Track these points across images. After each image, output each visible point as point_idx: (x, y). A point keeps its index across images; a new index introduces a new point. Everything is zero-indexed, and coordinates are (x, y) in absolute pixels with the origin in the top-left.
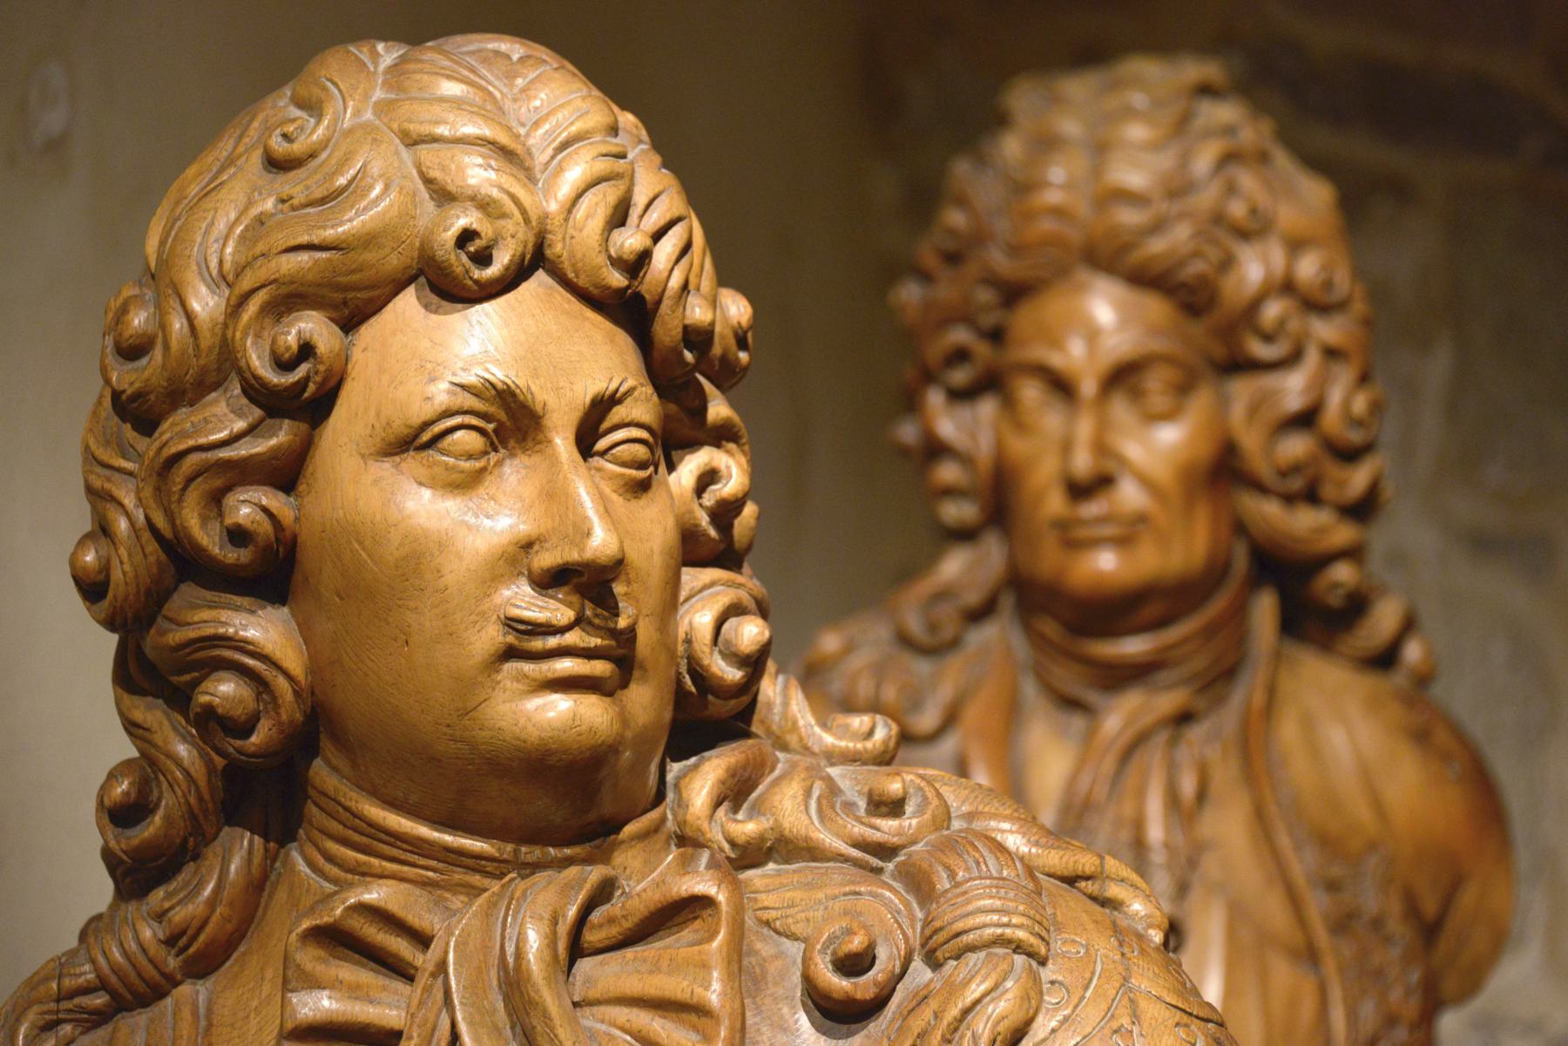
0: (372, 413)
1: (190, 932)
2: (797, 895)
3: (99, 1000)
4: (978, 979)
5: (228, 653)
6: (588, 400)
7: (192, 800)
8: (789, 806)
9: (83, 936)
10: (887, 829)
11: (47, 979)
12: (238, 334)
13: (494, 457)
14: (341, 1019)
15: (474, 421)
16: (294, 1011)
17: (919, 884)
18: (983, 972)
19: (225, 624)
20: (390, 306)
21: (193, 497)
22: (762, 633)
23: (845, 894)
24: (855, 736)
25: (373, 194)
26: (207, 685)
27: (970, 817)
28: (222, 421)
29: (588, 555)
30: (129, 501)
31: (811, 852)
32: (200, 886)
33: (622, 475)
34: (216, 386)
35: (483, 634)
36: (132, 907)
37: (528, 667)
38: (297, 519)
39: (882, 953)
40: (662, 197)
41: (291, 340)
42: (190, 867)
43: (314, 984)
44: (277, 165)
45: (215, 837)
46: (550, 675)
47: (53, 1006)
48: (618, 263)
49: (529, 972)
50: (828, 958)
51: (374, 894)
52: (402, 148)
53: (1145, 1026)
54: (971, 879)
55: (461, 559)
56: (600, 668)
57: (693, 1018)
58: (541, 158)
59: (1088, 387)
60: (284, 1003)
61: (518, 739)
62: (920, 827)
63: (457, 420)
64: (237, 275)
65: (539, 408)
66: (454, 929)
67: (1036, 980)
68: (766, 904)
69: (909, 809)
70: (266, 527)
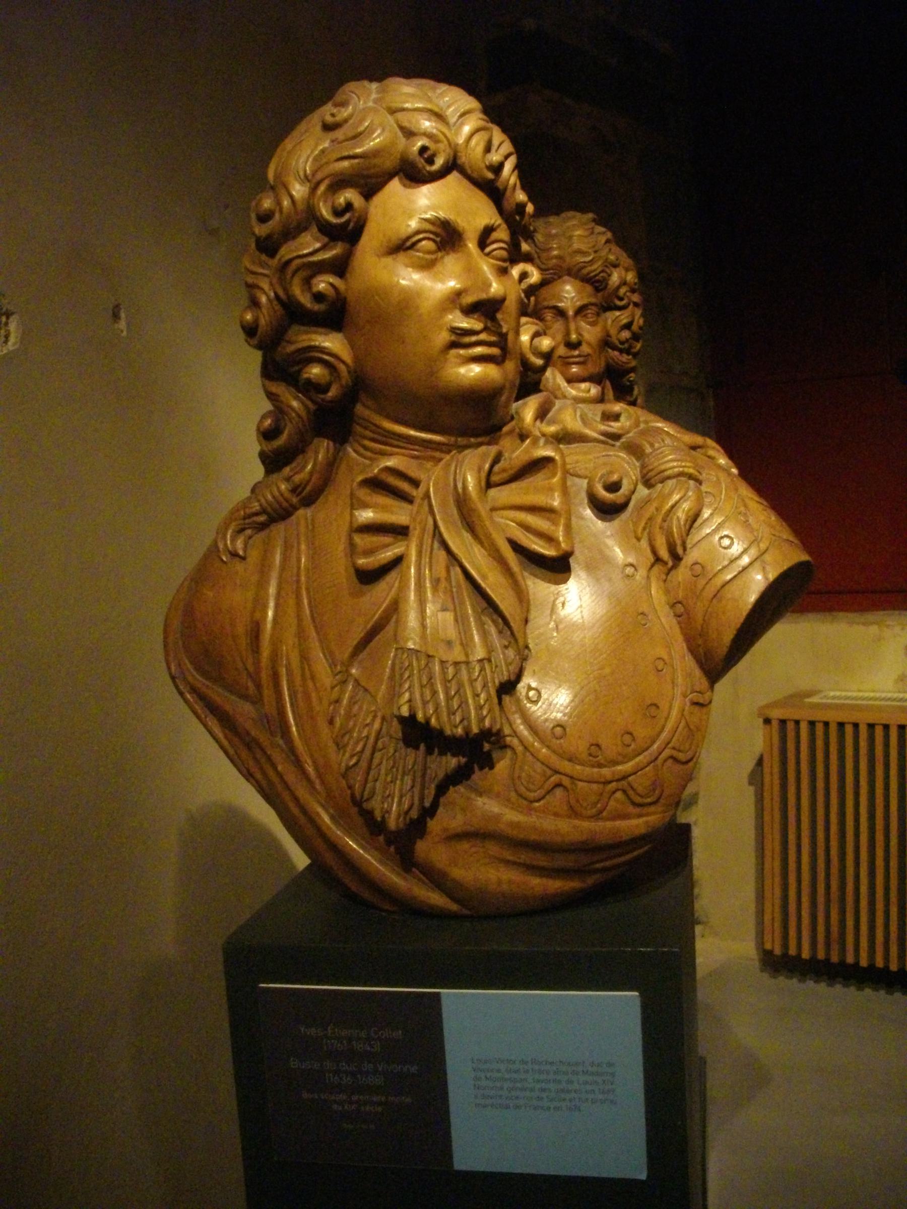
0: (381, 235)
2: (580, 457)
3: (262, 518)
4: (676, 492)
6: (482, 227)
7: (300, 425)
8: (569, 418)
9: (253, 490)
10: (615, 427)
11: (238, 510)
13: (440, 254)
14: (379, 522)
15: (431, 236)
16: (357, 520)
17: (634, 450)
19: (314, 340)
24: (583, 391)
26: (307, 369)
27: (646, 422)
28: (309, 244)
30: (266, 287)
31: (581, 439)
32: (304, 467)
34: (306, 229)
36: (275, 476)
37: (462, 352)
39: (625, 482)
41: (342, 200)
42: (301, 457)
43: (365, 506)
44: (328, 128)
45: (311, 443)
46: (473, 355)
47: (242, 522)
51: (390, 463)
52: (388, 116)
56: (495, 351)
57: (548, 515)
59: (571, 313)
60: (352, 515)
62: (630, 427)
63: (421, 236)
66: (433, 478)
67: (699, 490)
69: (622, 419)
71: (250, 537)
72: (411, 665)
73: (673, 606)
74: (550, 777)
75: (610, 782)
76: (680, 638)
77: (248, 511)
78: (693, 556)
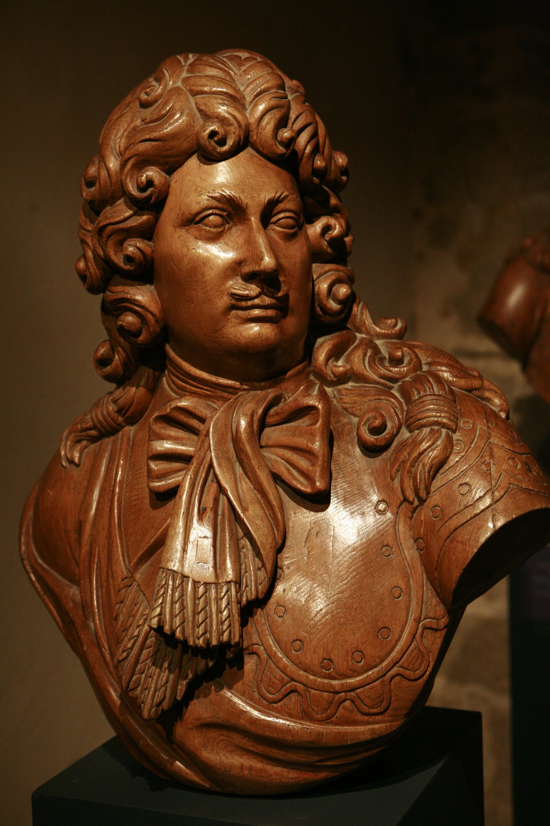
0: (178, 208)
1: (126, 409)
2: (357, 399)
3: (93, 432)
5: (128, 305)
8: (358, 361)
12: (123, 177)
13: (227, 226)
18: (428, 438)
20: (186, 163)
21: (110, 243)
22: (347, 291)
23: (376, 399)
25: (176, 118)
26: (122, 317)
28: (122, 211)
29: (262, 268)
33: (283, 232)
35: (222, 300)
37: (241, 313)
38: (152, 252)
39: (389, 425)
40: (303, 115)
41: (144, 178)
43: (162, 438)
44: (145, 105)
48: (281, 143)
49: (240, 438)
50: (367, 428)
51: (183, 403)
53: (496, 459)
54: (427, 395)
55: (212, 269)
57: (308, 455)
58: (248, 99)
61: (237, 342)
64: (125, 151)
65: (244, 205)
66: (215, 417)
68: (345, 401)
70: (139, 254)
71: (86, 447)
72: (167, 583)
73: (416, 540)
74: (287, 684)
75: (339, 693)
76: (420, 568)
77: (84, 426)
78: (435, 499)
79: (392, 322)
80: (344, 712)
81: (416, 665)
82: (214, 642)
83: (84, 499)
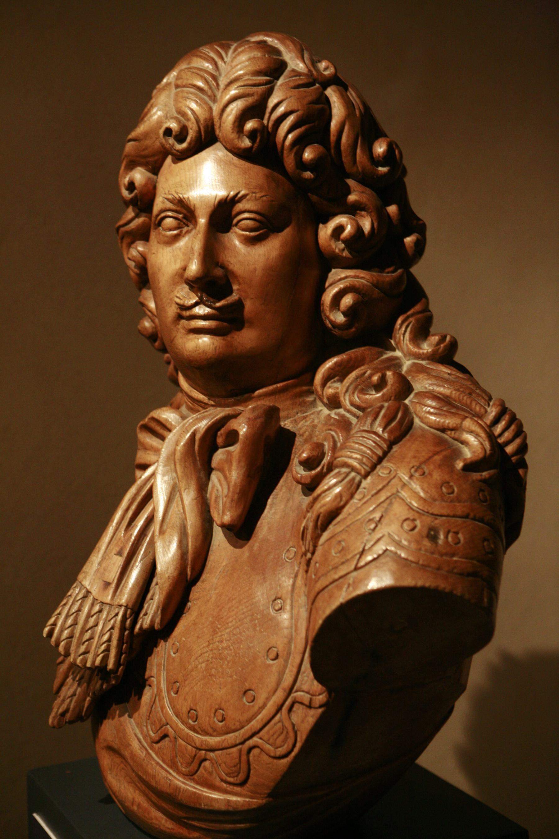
13: (185, 229)
65: (192, 208)
79: (435, 339)
80: (203, 771)
81: (279, 742)
82: (89, 665)
83: (360, 507)
